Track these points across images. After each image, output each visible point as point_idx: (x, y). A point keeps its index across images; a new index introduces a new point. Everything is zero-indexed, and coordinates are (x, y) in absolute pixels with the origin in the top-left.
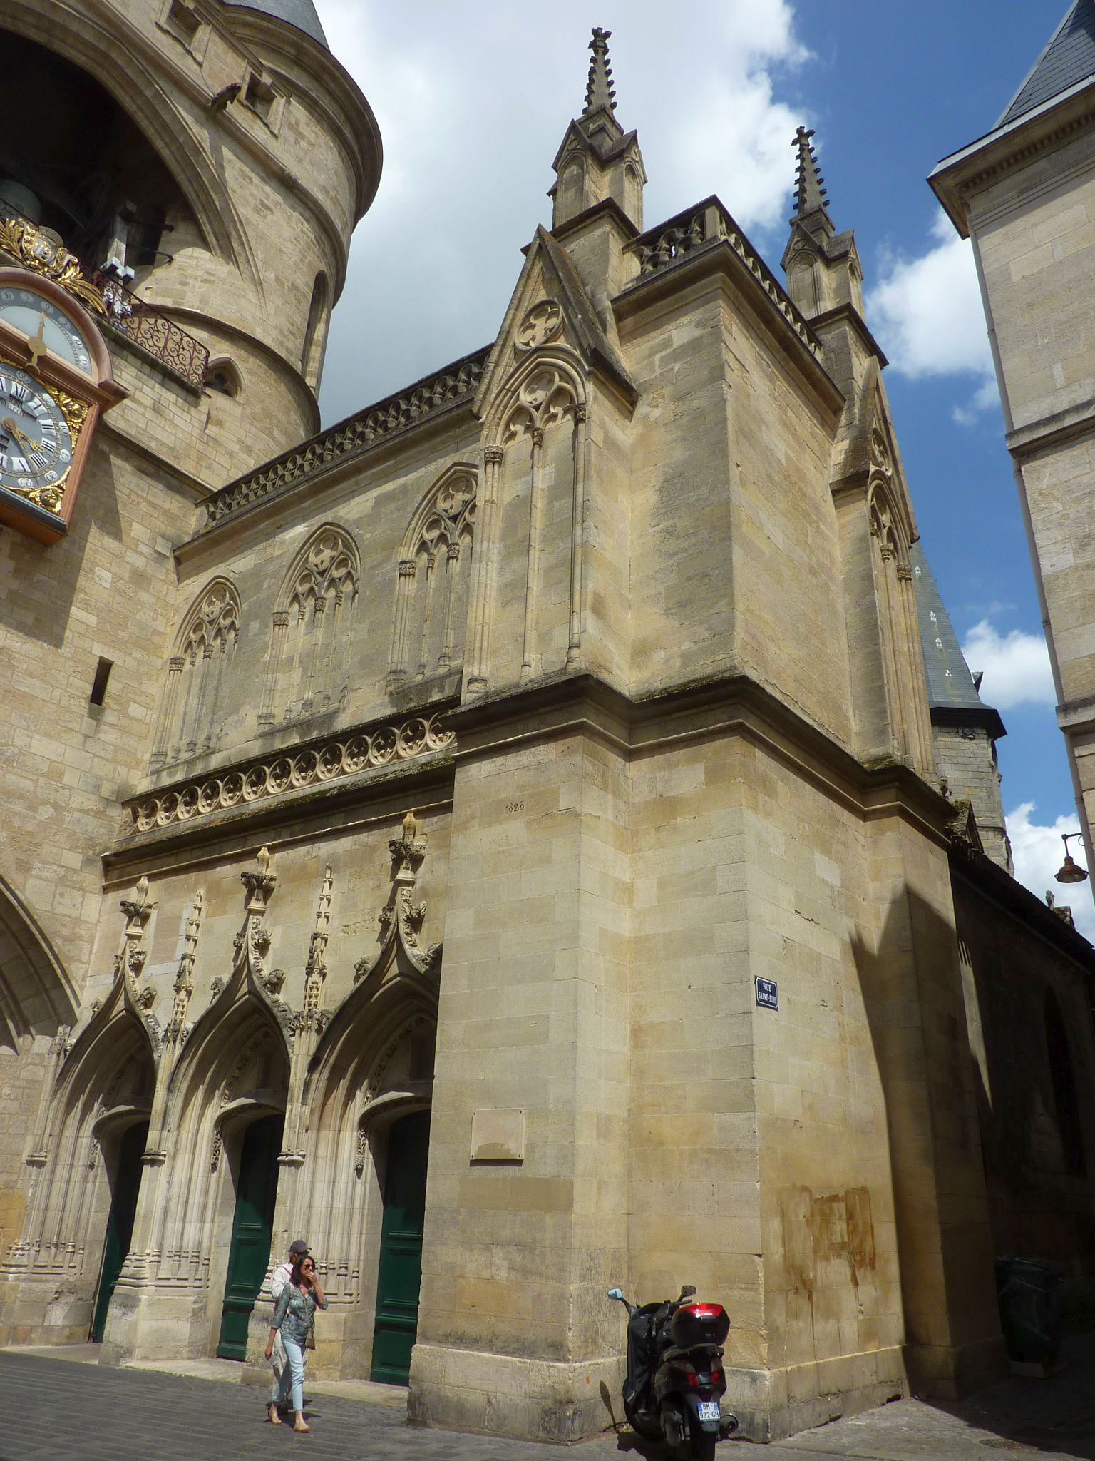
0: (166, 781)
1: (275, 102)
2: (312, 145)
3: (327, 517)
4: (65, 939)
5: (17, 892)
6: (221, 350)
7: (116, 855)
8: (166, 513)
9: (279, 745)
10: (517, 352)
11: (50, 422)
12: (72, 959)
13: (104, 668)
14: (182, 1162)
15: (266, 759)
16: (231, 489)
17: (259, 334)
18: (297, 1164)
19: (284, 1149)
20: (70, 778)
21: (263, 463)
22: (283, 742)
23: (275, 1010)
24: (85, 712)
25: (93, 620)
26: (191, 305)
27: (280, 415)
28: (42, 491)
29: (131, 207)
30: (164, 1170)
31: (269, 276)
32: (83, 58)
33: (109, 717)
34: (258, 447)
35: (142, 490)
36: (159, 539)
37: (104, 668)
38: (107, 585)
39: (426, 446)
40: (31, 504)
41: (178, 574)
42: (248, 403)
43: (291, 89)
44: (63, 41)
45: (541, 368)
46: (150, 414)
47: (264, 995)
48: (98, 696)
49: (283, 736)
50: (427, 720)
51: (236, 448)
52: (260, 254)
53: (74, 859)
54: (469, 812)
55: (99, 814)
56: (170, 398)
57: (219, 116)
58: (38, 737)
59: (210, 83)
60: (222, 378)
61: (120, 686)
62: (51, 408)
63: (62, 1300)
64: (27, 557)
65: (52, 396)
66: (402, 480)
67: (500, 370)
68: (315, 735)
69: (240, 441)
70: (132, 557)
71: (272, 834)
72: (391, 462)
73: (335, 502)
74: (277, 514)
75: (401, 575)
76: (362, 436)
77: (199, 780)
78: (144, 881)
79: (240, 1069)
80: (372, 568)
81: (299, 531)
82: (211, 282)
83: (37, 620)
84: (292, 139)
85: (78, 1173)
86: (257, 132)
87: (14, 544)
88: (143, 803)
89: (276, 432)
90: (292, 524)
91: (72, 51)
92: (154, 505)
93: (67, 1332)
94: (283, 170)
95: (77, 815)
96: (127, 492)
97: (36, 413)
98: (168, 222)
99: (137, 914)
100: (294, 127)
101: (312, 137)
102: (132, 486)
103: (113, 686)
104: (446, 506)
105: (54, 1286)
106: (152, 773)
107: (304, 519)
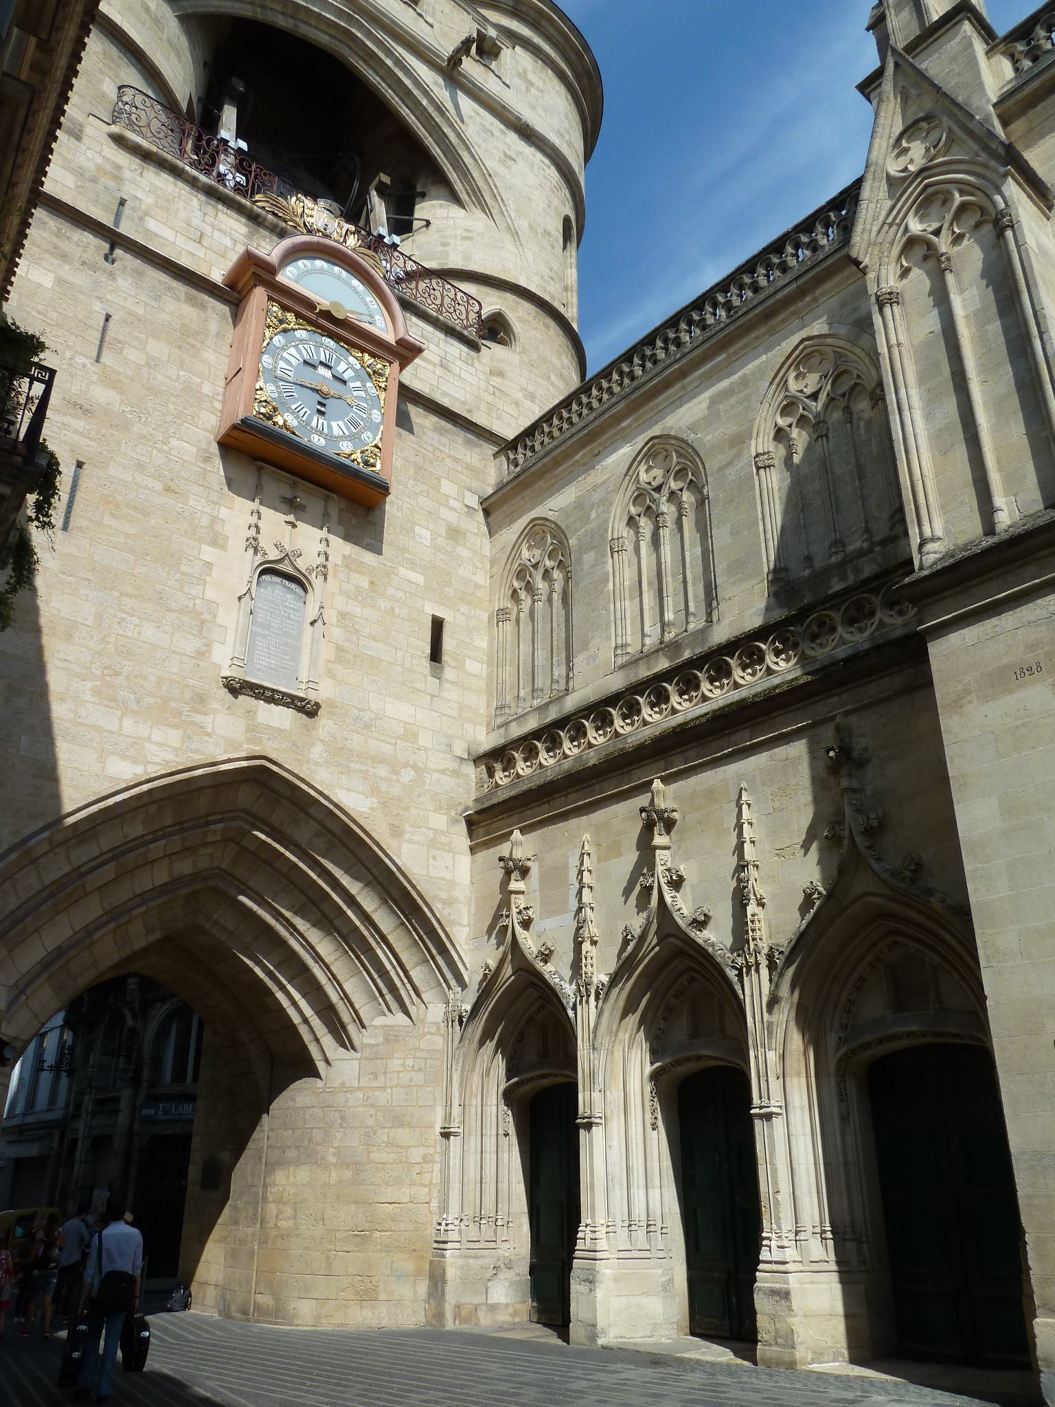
0: (517, 731)
1: (502, 53)
2: (542, 91)
3: (656, 430)
4: (444, 902)
5: (394, 857)
6: (492, 302)
7: (478, 812)
8: (468, 467)
9: (644, 672)
10: (891, 181)
11: (358, 384)
12: (453, 923)
13: (438, 626)
14: (616, 1125)
15: (638, 688)
16: (530, 432)
17: (522, 282)
18: (768, 1117)
19: (756, 1101)
20: (424, 740)
21: (547, 409)
22: (649, 669)
23: (710, 950)
24: (427, 671)
25: (420, 579)
26: (456, 262)
27: (555, 360)
28: (362, 452)
29: (386, 179)
30: (778, 1123)
31: (522, 224)
32: (327, 38)
33: (449, 673)
34: (540, 392)
35: (444, 446)
36: (466, 493)
37: (438, 626)
38: (428, 543)
39: (763, 329)
40: (355, 465)
41: (488, 525)
42: (524, 351)
43: (516, 39)
44: (309, 25)
45: (930, 190)
46: (439, 371)
47: (692, 935)
48: (436, 654)
49: (648, 663)
50: (732, 657)
51: (519, 396)
52: (511, 205)
53: (440, 821)
54: (960, 687)
55: (456, 773)
56: (456, 349)
57: (455, 74)
58: (389, 700)
59: (443, 43)
60: (495, 329)
61: (454, 642)
62: (356, 371)
63: (501, 1276)
64: (354, 521)
65: (356, 358)
66: (740, 374)
67: (875, 204)
68: (687, 654)
69: (523, 389)
70: (445, 513)
71: (662, 764)
72: (723, 356)
73: (660, 415)
74: (594, 439)
75: (758, 468)
76: (678, 343)
77: (561, 723)
78: (517, 834)
79: (665, 1019)
80: (720, 469)
81: (625, 452)
82: (470, 238)
83: (372, 583)
84: (524, 88)
85: (490, 1143)
86: (491, 85)
87: (341, 510)
88: (497, 757)
89: (553, 378)
90: (612, 447)
91: (318, 33)
92: (456, 460)
93: (511, 1309)
94: (519, 119)
95: (436, 775)
96: (431, 449)
97: (346, 376)
98: (419, 189)
99: (515, 869)
100: (522, 76)
101: (540, 84)
102: (435, 444)
103: (448, 643)
104: (800, 386)
105: (490, 1262)
106: (499, 727)
107: (626, 438)
